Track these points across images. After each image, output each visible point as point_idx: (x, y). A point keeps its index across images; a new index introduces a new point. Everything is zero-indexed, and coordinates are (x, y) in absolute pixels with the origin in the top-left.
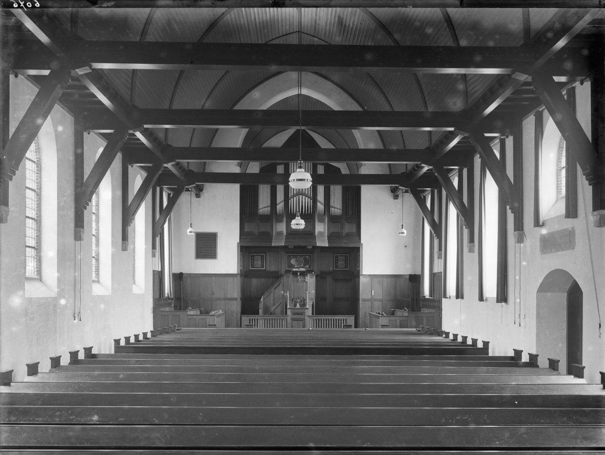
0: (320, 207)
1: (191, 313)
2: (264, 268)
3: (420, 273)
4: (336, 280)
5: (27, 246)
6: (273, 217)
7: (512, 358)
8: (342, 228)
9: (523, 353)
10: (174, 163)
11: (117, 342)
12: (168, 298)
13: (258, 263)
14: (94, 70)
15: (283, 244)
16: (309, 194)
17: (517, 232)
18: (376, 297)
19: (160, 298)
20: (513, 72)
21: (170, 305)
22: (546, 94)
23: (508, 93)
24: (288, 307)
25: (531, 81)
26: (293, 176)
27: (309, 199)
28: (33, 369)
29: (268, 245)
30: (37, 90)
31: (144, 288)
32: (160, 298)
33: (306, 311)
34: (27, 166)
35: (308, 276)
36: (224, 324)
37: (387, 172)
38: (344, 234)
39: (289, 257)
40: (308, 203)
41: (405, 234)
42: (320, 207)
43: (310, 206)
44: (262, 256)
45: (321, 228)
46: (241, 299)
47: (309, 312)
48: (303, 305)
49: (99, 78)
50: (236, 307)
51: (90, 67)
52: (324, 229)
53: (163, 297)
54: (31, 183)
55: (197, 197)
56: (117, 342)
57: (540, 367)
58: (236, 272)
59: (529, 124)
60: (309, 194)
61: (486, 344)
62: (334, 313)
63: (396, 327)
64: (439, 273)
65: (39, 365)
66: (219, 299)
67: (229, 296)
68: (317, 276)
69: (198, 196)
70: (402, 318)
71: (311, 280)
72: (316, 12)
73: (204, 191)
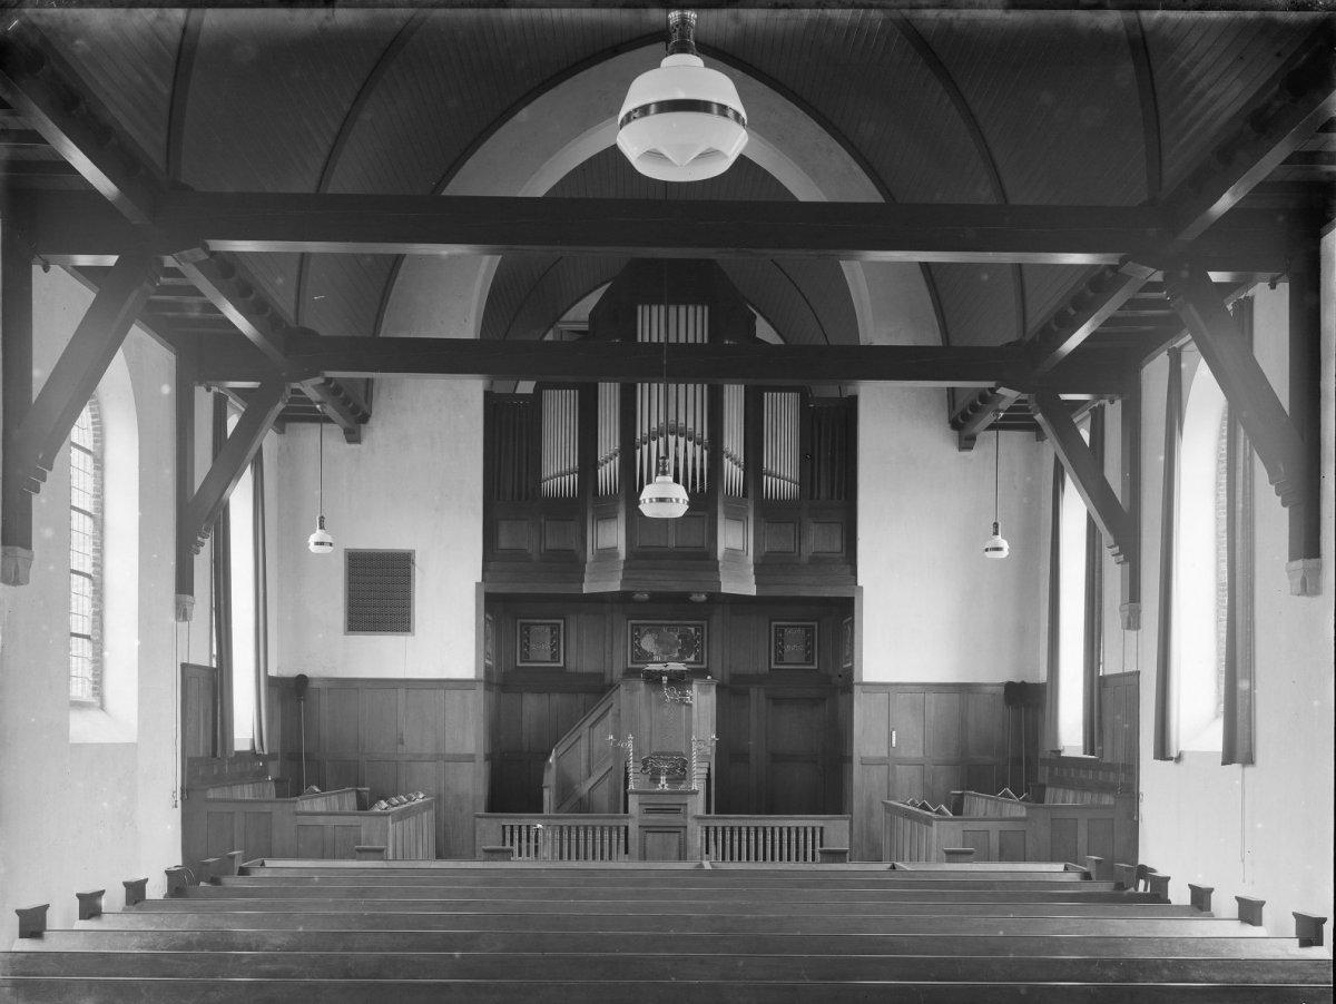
0: (733, 472)
1: (319, 805)
2: (561, 664)
3: (1043, 677)
4: (777, 701)
5: (73, 635)
6: (586, 502)
8: (800, 537)
9: (1170, 883)
10: (320, 380)
12: (252, 755)
13: (541, 651)
14: (213, 254)
15: (615, 586)
16: (698, 431)
17: (1299, 564)
18: (903, 753)
19: (214, 755)
20: (998, 387)
21: (260, 776)
22: (1191, 307)
23: (1108, 309)
24: (631, 786)
25: (1162, 280)
26: (648, 493)
27: (698, 448)
28: (90, 906)
29: (570, 589)
30: (92, 296)
31: (134, 722)
32: (214, 755)
33: (690, 800)
34: (74, 461)
35: (694, 687)
36: (428, 840)
38: (804, 559)
39: (636, 628)
40: (694, 459)
41: (1005, 554)
42: (733, 472)
43: (702, 470)
44: (554, 628)
45: (733, 538)
46: (489, 757)
47: (697, 805)
48: (680, 772)
49: (228, 272)
50: (472, 782)
51: (205, 248)
52: (746, 540)
53: (224, 750)
54: (82, 498)
55: (349, 441)
57: (1173, 903)
58: (471, 675)
59: (1155, 373)
60: (698, 431)
62: (772, 809)
63: (988, 859)
64: (1131, 674)
65: (49, 913)
66: (419, 758)
67: (450, 749)
68: (720, 688)
69: (353, 436)
70: (1007, 826)
71: (702, 700)
72: (636, 793)
73: (372, 421)
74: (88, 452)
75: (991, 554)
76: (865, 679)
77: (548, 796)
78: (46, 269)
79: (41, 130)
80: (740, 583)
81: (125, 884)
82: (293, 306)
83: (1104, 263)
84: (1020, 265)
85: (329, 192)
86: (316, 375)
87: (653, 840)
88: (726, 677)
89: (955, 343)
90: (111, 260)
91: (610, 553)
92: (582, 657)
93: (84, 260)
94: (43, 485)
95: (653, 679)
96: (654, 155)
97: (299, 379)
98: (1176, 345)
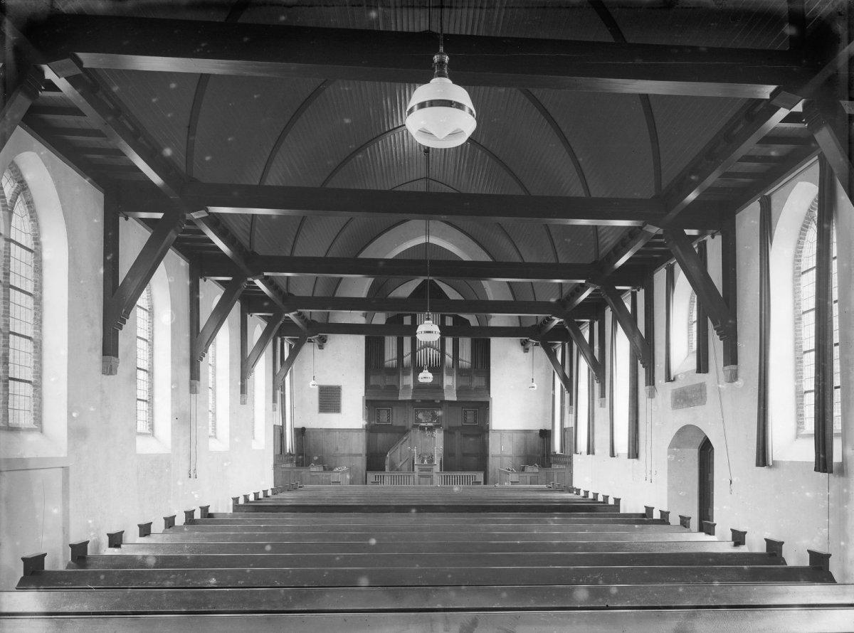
0: (449, 360)
1: (314, 469)
7: (643, 515)
8: (471, 381)
9: (621, 501)
10: (296, 313)
11: (236, 500)
13: (384, 418)
15: (410, 398)
20: (644, 225)
25: (801, 111)
26: (421, 328)
28: (145, 530)
29: (395, 399)
33: (434, 467)
37: (518, 325)
41: (536, 388)
42: (449, 360)
45: (449, 381)
46: (367, 455)
47: (437, 468)
48: (431, 461)
49: (217, 223)
50: (361, 463)
51: (207, 210)
56: (236, 500)
59: (660, 276)
61: (617, 501)
65: (152, 526)
66: (343, 455)
67: (354, 452)
69: (321, 347)
70: (533, 475)
71: (439, 436)
74: (146, 310)
75: (531, 389)
76: (493, 428)
77: (387, 468)
78: (127, 219)
79: (124, 151)
80: (451, 396)
81: (139, 526)
82: (285, 284)
83: (635, 225)
84: (596, 226)
85: (266, 184)
86: (317, 334)
87: (423, 480)
88: (447, 428)
89: (537, 300)
90: (159, 215)
91: (408, 387)
92: (398, 421)
93: (144, 215)
94: (124, 326)
95: (422, 428)
96: (425, 132)
97: (288, 313)
98: (766, 194)
